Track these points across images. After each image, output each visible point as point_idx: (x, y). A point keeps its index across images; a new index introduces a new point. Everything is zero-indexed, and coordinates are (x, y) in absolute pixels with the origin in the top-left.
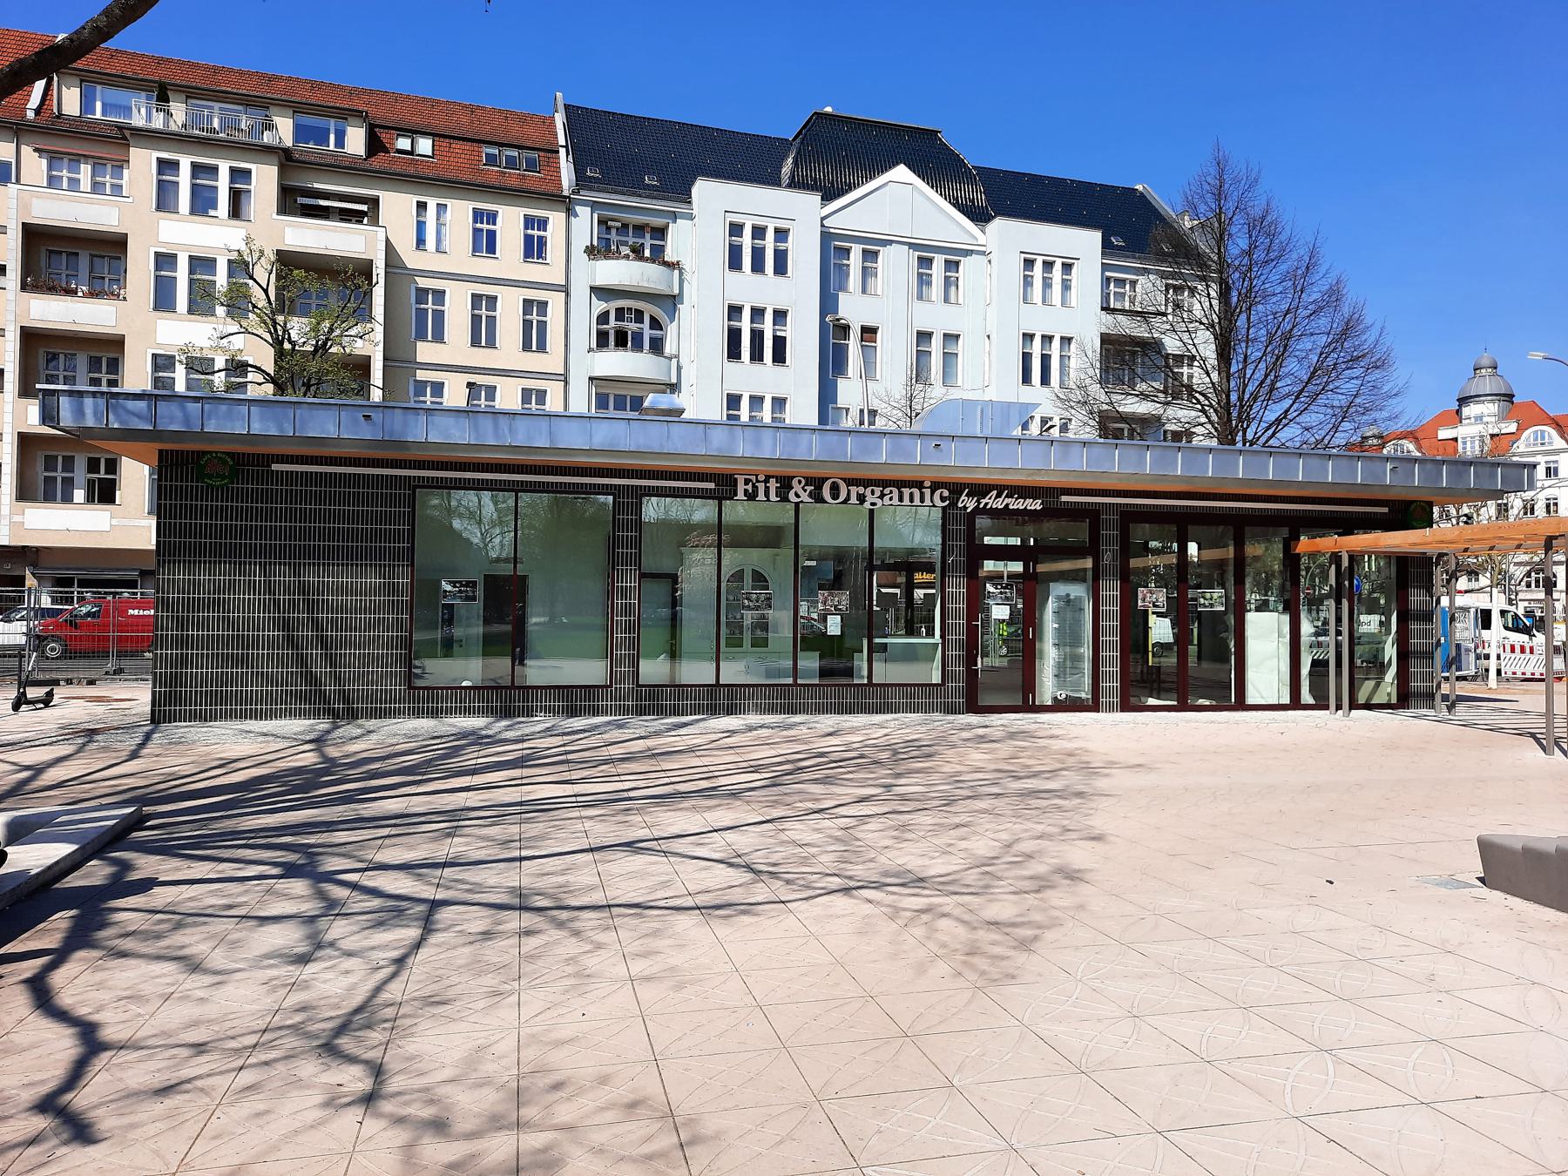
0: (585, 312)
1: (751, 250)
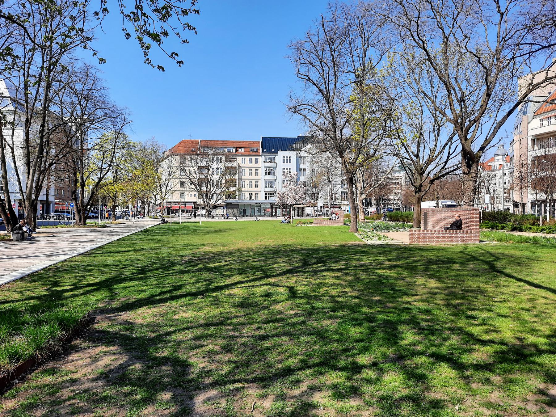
1: (286, 160)
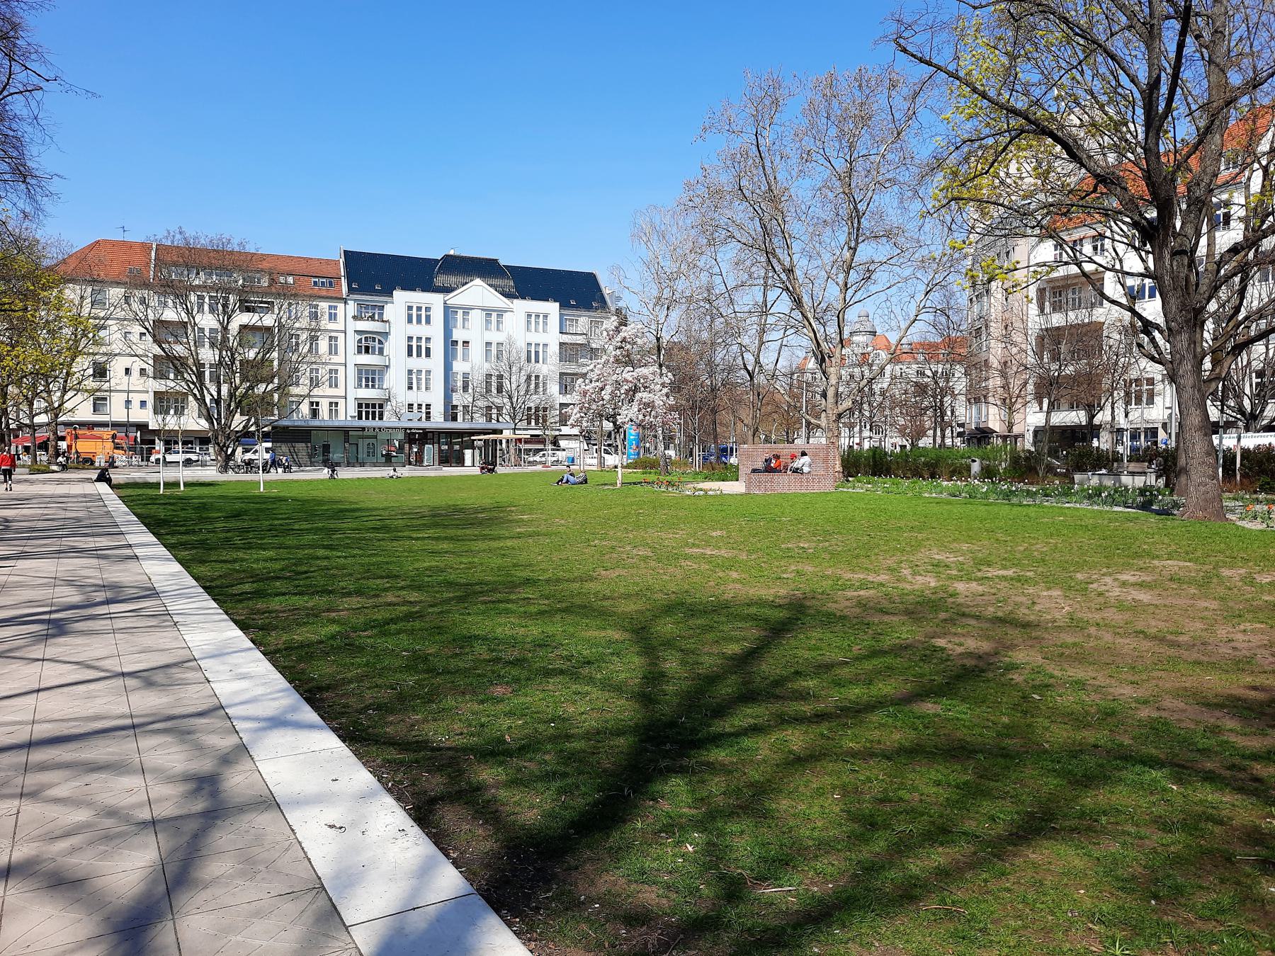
1: (416, 315)
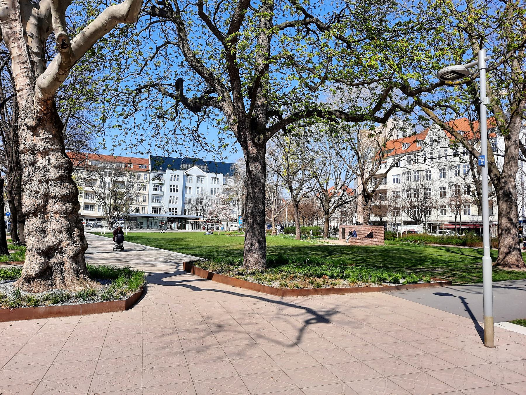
0: (151, 197)
1: (174, 178)
